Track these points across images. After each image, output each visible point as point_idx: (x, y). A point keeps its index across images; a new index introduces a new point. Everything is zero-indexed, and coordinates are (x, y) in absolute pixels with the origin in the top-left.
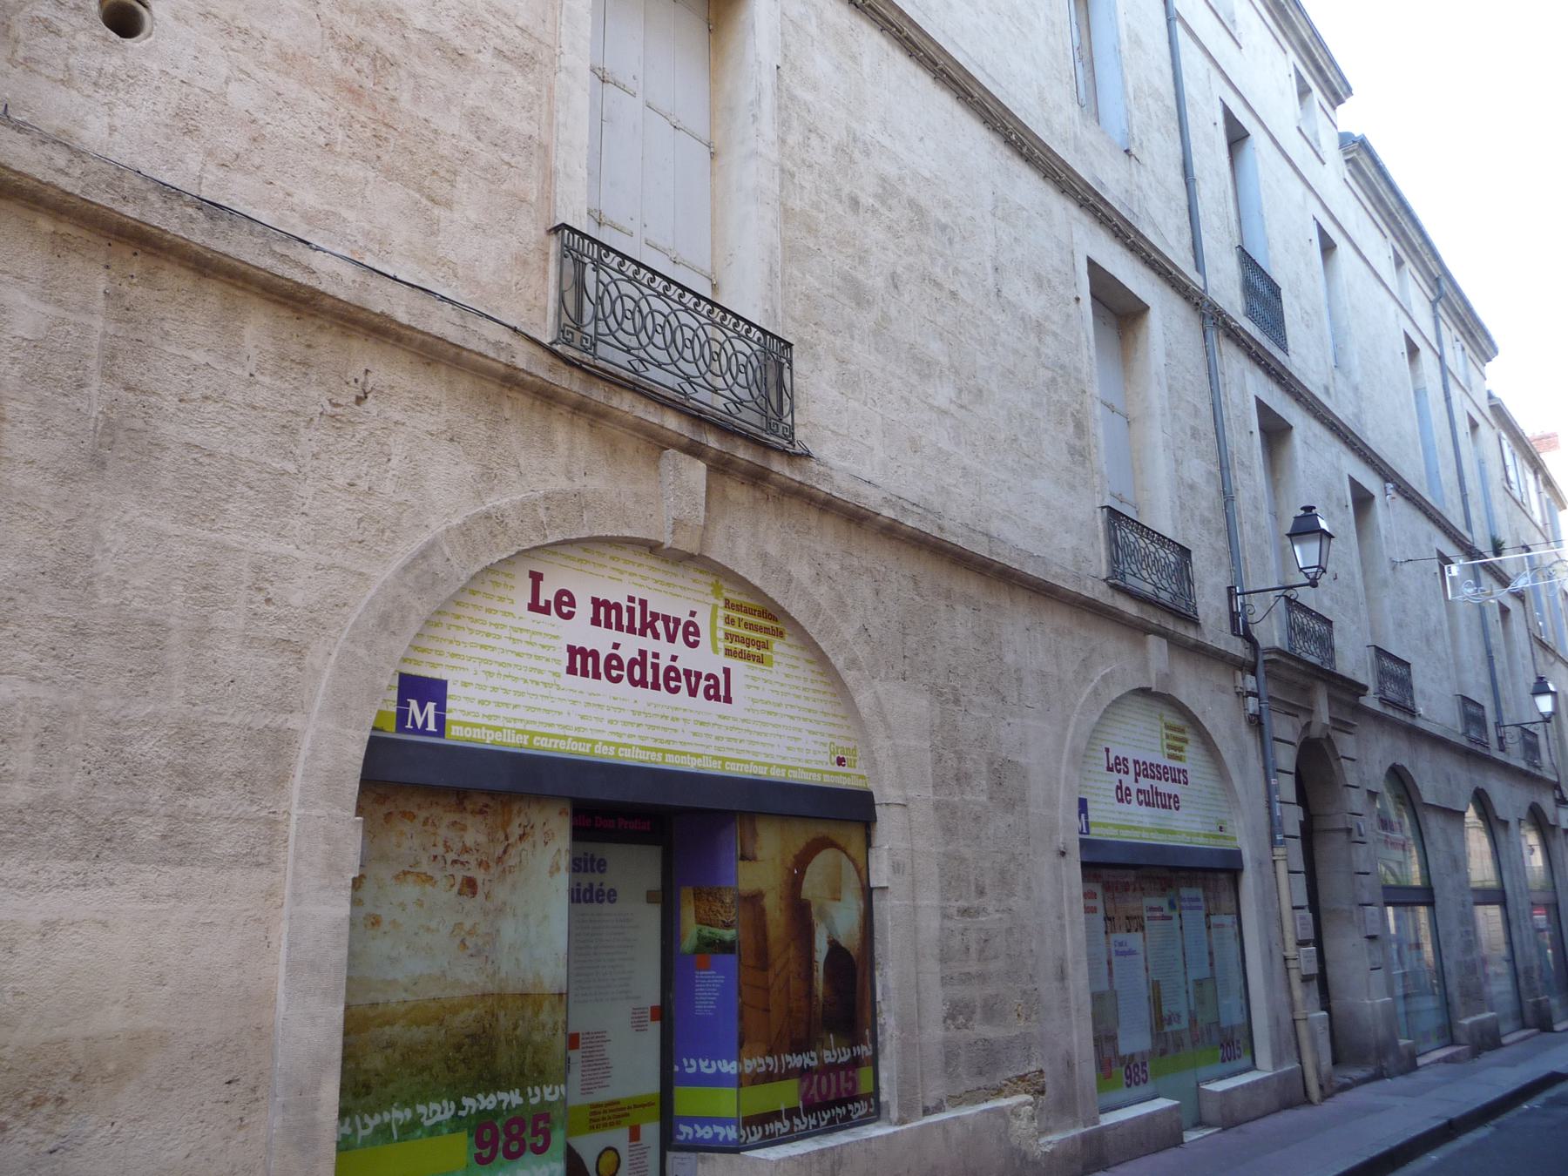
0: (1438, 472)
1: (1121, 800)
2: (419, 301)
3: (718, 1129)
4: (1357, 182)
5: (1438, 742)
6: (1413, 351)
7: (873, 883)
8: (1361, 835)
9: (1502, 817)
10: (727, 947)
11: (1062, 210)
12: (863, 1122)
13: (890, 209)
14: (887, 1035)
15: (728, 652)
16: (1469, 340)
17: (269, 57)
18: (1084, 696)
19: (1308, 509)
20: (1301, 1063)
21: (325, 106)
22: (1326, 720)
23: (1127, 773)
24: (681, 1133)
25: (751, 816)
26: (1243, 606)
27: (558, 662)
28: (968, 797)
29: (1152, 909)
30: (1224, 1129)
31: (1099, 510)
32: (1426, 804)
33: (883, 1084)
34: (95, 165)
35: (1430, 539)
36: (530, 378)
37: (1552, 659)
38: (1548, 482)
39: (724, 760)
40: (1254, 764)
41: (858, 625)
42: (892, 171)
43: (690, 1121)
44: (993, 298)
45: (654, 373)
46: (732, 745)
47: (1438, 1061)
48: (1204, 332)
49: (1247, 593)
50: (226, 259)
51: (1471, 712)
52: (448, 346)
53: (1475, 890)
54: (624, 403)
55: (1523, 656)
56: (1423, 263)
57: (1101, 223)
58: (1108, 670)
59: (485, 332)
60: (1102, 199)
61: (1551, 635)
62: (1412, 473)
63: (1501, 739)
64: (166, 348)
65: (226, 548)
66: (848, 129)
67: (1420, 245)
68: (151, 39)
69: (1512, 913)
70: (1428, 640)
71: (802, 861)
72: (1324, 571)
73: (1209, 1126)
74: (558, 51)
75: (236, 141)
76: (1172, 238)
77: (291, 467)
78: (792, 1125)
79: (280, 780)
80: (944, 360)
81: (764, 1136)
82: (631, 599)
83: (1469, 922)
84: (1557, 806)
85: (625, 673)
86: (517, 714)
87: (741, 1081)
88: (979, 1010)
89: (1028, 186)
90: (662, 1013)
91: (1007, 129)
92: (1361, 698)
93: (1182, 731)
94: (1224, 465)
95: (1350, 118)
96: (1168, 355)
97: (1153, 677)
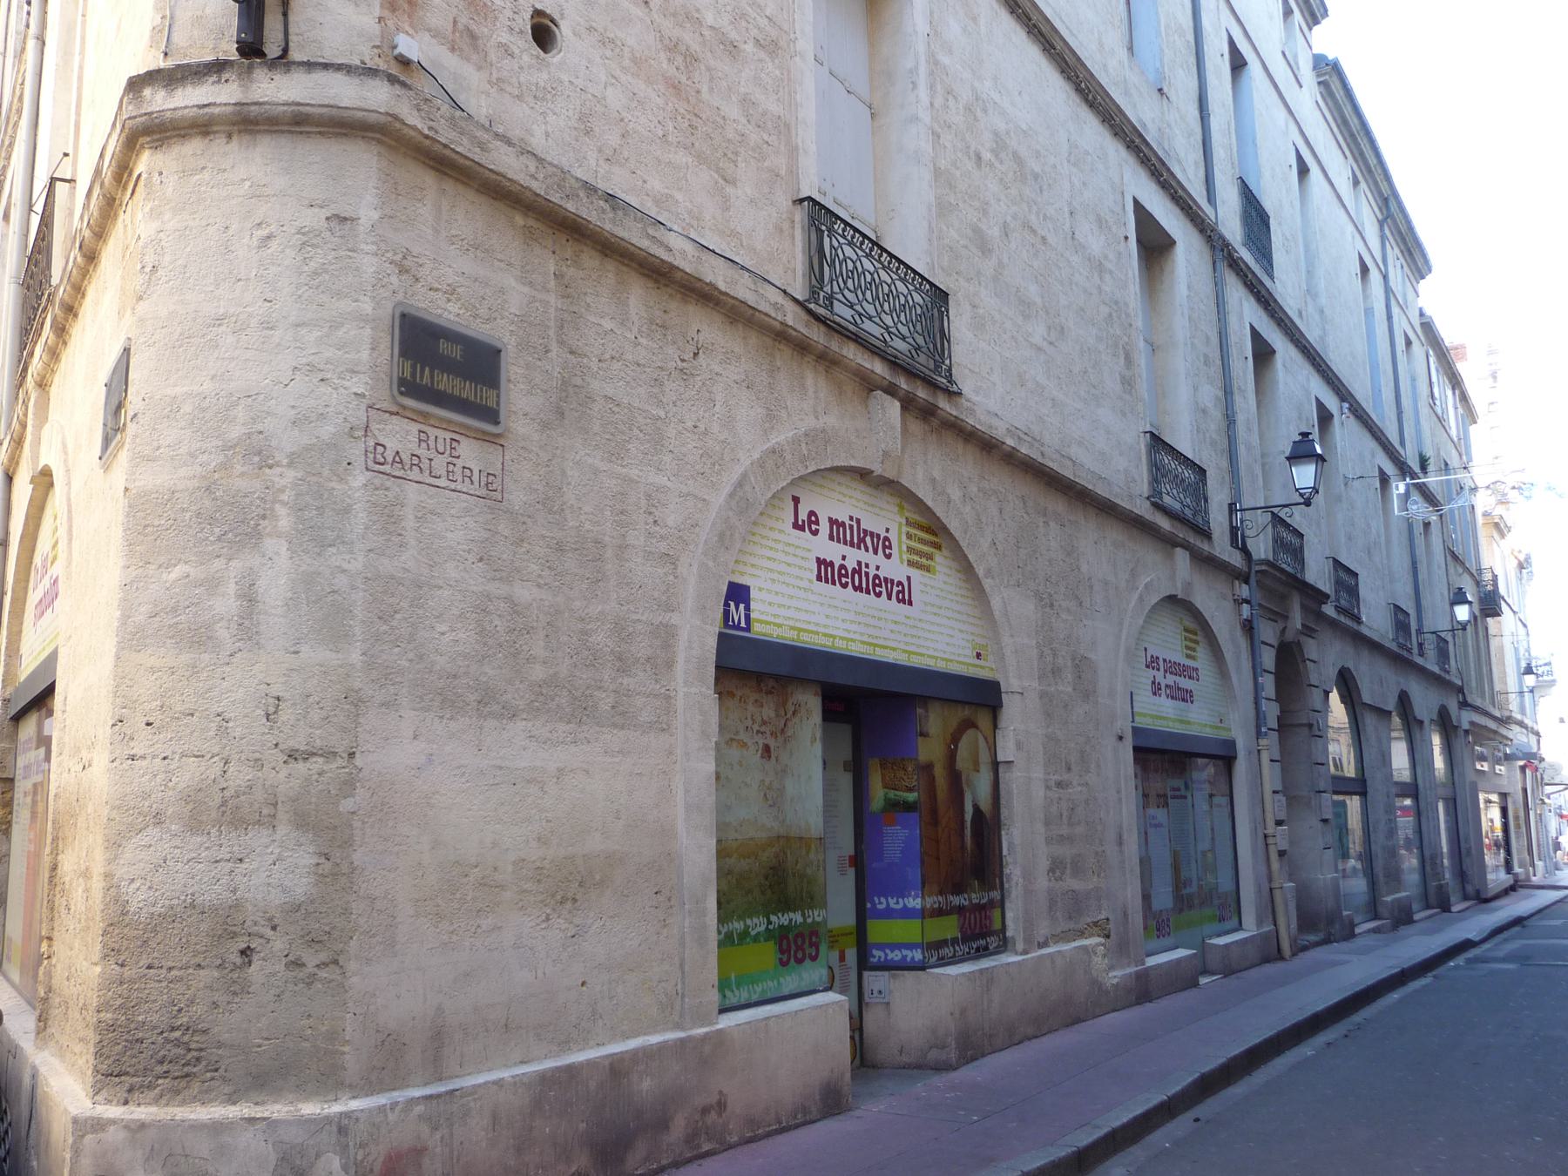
0: (1380, 391)
1: (1155, 694)
2: (732, 272)
3: (905, 952)
4: (1327, 104)
5: (1374, 646)
6: (1365, 270)
7: (1000, 758)
8: (1320, 730)
9: (1419, 718)
10: (909, 807)
11: (1115, 152)
12: (997, 952)
13: (1001, 162)
14: (1013, 883)
15: (911, 563)
16: (1407, 257)
17: (627, 63)
18: (1133, 603)
19: (1305, 435)
20: (1275, 925)
21: (660, 101)
22: (1299, 626)
23: (1158, 670)
24: (875, 957)
25: (925, 700)
26: (1242, 522)
27: (811, 570)
28: (1061, 688)
29: (1174, 789)
30: (1225, 977)
31: (1142, 435)
32: (1365, 704)
33: (1009, 922)
34: (550, 169)
35: (1373, 456)
36: (794, 333)
37: (1461, 570)
38: (1464, 398)
39: (910, 653)
40: (1246, 665)
41: (990, 540)
42: (1001, 126)
43: (881, 947)
44: (1069, 241)
45: (868, 325)
46: (914, 640)
47: (1369, 931)
48: (1214, 263)
49: (1244, 510)
50: (622, 242)
51: (1400, 619)
52: (747, 308)
53: (1397, 783)
54: (851, 352)
55: (1439, 567)
56: (1376, 183)
57: (1142, 162)
58: (1149, 579)
59: (768, 295)
60: (1145, 141)
61: (1461, 547)
62: (1361, 392)
63: (1420, 645)
64: (588, 317)
65: (632, 481)
66: (973, 89)
67: (1375, 166)
68: (562, 54)
69: (1422, 804)
70: (1369, 552)
71: (955, 739)
72: (1317, 492)
73: (1213, 974)
74: (792, 36)
75: (613, 139)
76: (1191, 171)
77: (662, 414)
78: (955, 951)
79: (670, 664)
80: (1038, 300)
81: (939, 959)
82: (851, 518)
83: (1390, 810)
84: (1460, 708)
85: (849, 580)
86: (790, 613)
87: (923, 914)
88: (1068, 866)
89: (1092, 131)
90: (857, 861)
91: (1078, 77)
92: (1323, 606)
93: (1196, 634)
94: (1228, 390)
95: (1326, 39)
96: (1189, 287)
97: (1179, 585)
